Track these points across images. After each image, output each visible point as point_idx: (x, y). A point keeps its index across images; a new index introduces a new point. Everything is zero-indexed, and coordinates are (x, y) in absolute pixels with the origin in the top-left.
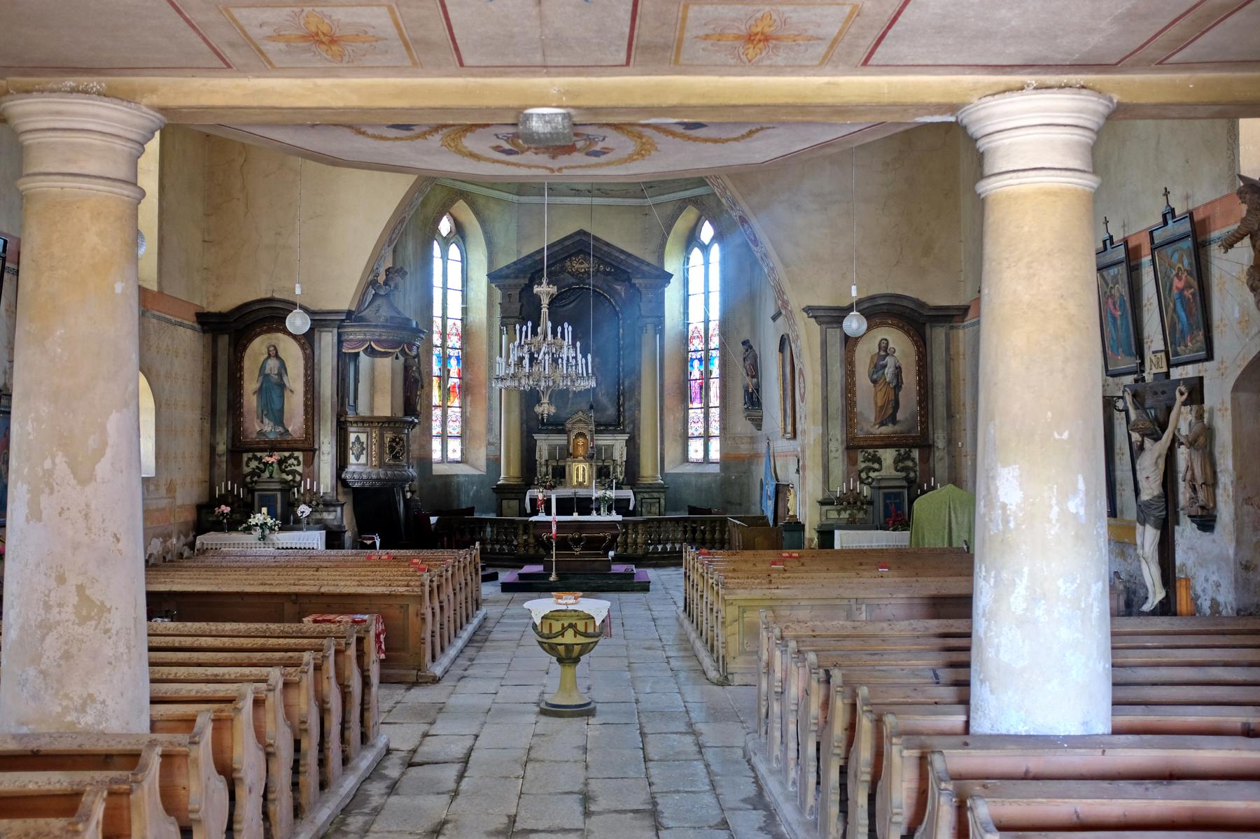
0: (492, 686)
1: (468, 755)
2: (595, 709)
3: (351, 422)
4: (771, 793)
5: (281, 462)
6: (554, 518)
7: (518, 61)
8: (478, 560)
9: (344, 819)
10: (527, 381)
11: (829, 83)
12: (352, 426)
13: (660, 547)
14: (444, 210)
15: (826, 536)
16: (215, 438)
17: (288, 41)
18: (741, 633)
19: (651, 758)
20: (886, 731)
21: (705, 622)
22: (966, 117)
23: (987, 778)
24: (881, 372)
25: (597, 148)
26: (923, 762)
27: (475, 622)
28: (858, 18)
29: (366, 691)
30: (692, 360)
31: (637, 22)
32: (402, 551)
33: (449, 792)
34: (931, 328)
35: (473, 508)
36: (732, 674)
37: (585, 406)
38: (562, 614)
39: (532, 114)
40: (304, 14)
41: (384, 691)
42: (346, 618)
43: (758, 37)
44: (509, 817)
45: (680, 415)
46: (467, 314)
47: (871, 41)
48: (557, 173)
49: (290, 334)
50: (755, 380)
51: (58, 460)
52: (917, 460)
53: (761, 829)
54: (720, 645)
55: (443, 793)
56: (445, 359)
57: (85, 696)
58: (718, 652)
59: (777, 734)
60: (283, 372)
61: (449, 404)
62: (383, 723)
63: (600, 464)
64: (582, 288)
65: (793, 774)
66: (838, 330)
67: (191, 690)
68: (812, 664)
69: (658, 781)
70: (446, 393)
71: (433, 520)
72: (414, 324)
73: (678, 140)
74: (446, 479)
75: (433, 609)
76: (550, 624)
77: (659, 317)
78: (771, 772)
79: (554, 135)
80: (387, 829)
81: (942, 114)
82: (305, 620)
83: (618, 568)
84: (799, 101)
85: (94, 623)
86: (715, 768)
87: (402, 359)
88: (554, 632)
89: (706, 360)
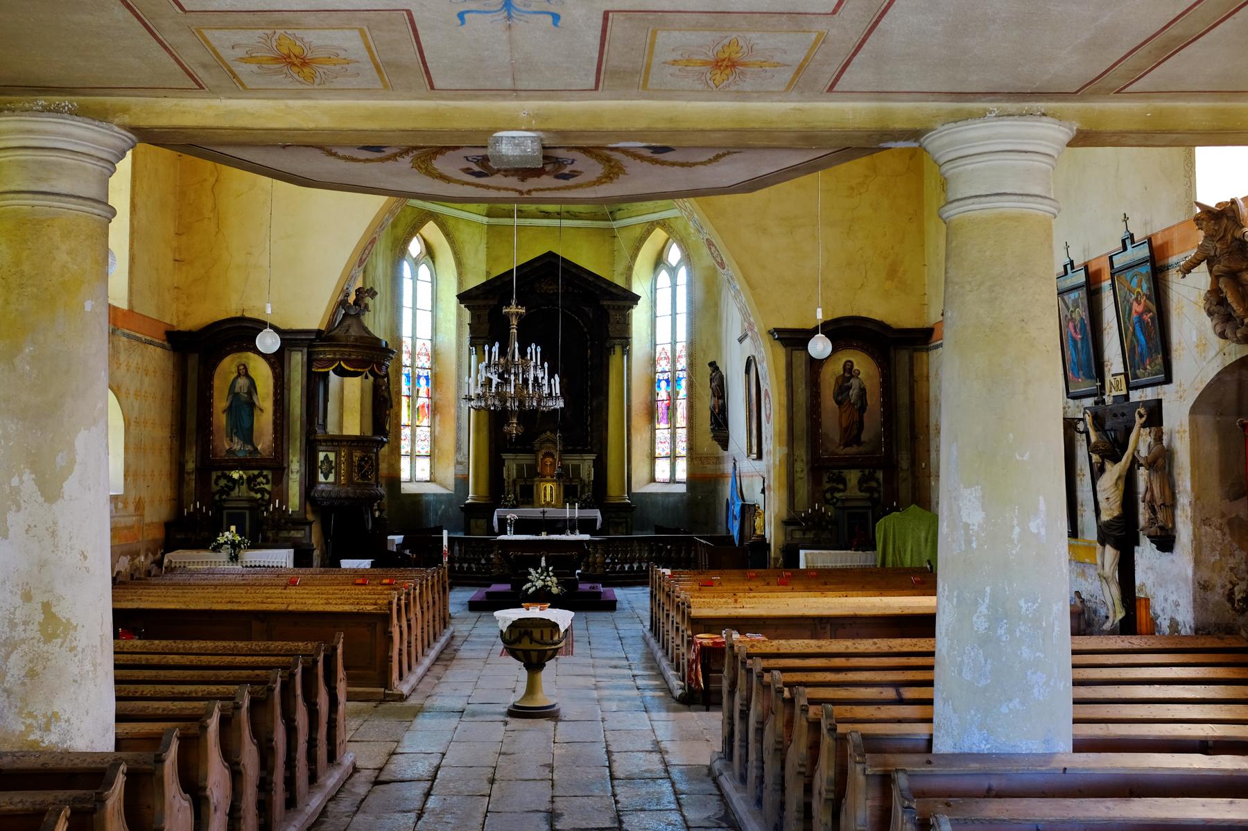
3: (320, 441)
7: (488, 85)
11: (794, 109)
12: (321, 445)
16: (184, 456)
24: (846, 394)
25: (566, 171)
27: (443, 640)
28: (823, 45)
30: (660, 381)
39: (502, 137)
40: (276, 36)
43: (725, 63)
45: (647, 435)
48: (526, 196)
50: (721, 401)
51: (25, 478)
56: (414, 379)
57: (49, 714)
60: (253, 390)
61: (418, 423)
62: (349, 741)
66: (804, 352)
67: (158, 708)
70: (415, 411)
73: (645, 163)
74: (416, 498)
75: (400, 627)
83: (584, 587)
85: (59, 640)
89: (673, 382)
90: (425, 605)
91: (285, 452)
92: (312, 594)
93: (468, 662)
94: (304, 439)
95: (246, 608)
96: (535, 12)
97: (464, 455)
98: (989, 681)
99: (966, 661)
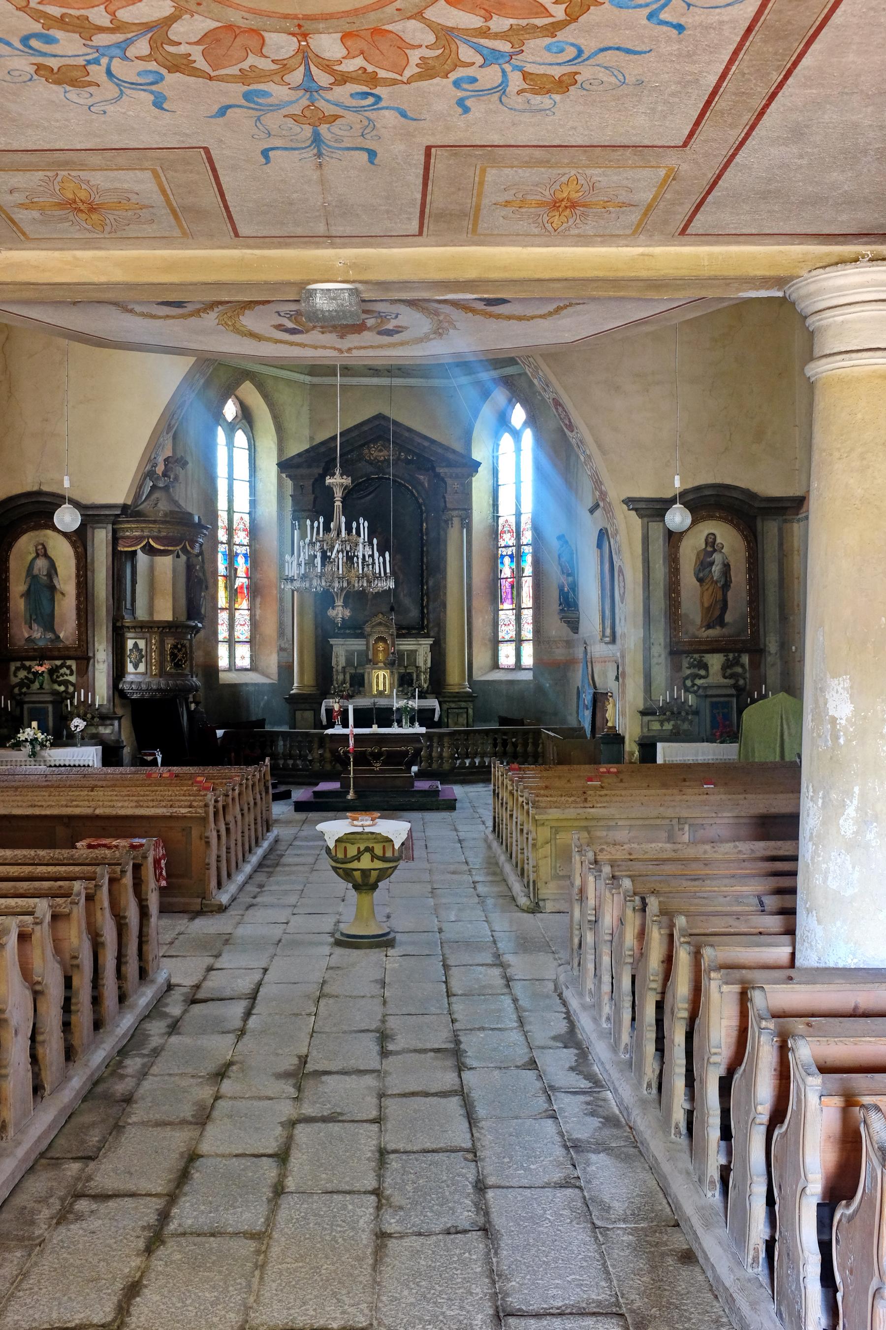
0: (282, 915)
1: (256, 991)
2: (394, 939)
3: (128, 627)
4: (583, 1029)
5: (52, 671)
6: (351, 730)
7: (299, 231)
8: (268, 777)
9: (121, 1062)
10: (319, 582)
11: (643, 255)
12: (129, 632)
13: (467, 762)
14: (228, 391)
15: (648, 749)
17: (42, 209)
18: (553, 855)
19: (454, 992)
20: (705, 964)
21: (514, 843)
22: (796, 292)
23: (813, 1016)
24: (708, 569)
25: (390, 326)
26: (744, 998)
27: (266, 844)
28: (674, 182)
29: (145, 922)
30: (503, 556)
31: (430, 187)
32: (184, 768)
33: (235, 1030)
34: (763, 522)
35: (264, 720)
36: (544, 900)
37: (385, 608)
38: (358, 836)
39: (316, 290)
40: (59, 178)
41: (166, 922)
42: (123, 843)
43: (564, 204)
44: (299, 1057)
45: (489, 617)
46: (255, 507)
47: (688, 207)
48: (346, 355)
49: (59, 531)
50: (570, 579)
52: (747, 667)
53: (572, 1069)
54: (531, 869)
55: (229, 1032)
56: (231, 557)
58: (528, 876)
59: (591, 966)
60: (53, 572)
61: (237, 606)
62: (164, 956)
63: (402, 671)
64: (382, 478)
65: (607, 1009)
66: (661, 524)
68: (627, 891)
69: (461, 1017)
70: (233, 594)
71: (220, 733)
72: (196, 519)
73: (478, 317)
74: (234, 688)
75: (218, 831)
76: (345, 848)
77: (465, 509)
78: (584, 1007)
79: (340, 313)
80: (167, 1071)
81: (768, 289)
82: (78, 844)
83: (422, 785)
84: (611, 275)
86: (523, 1003)
87: (183, 558)
88: (349, 856)
89: (517, 557)
90: (246, 808)
91: (90, 639)
92: (121, 796)
93: (294, 868)
94: (111, 625)
95: (48, 812)
96: (348, 149)
97: (288, 640)
98: (856, 890)
99: (832, 868)
